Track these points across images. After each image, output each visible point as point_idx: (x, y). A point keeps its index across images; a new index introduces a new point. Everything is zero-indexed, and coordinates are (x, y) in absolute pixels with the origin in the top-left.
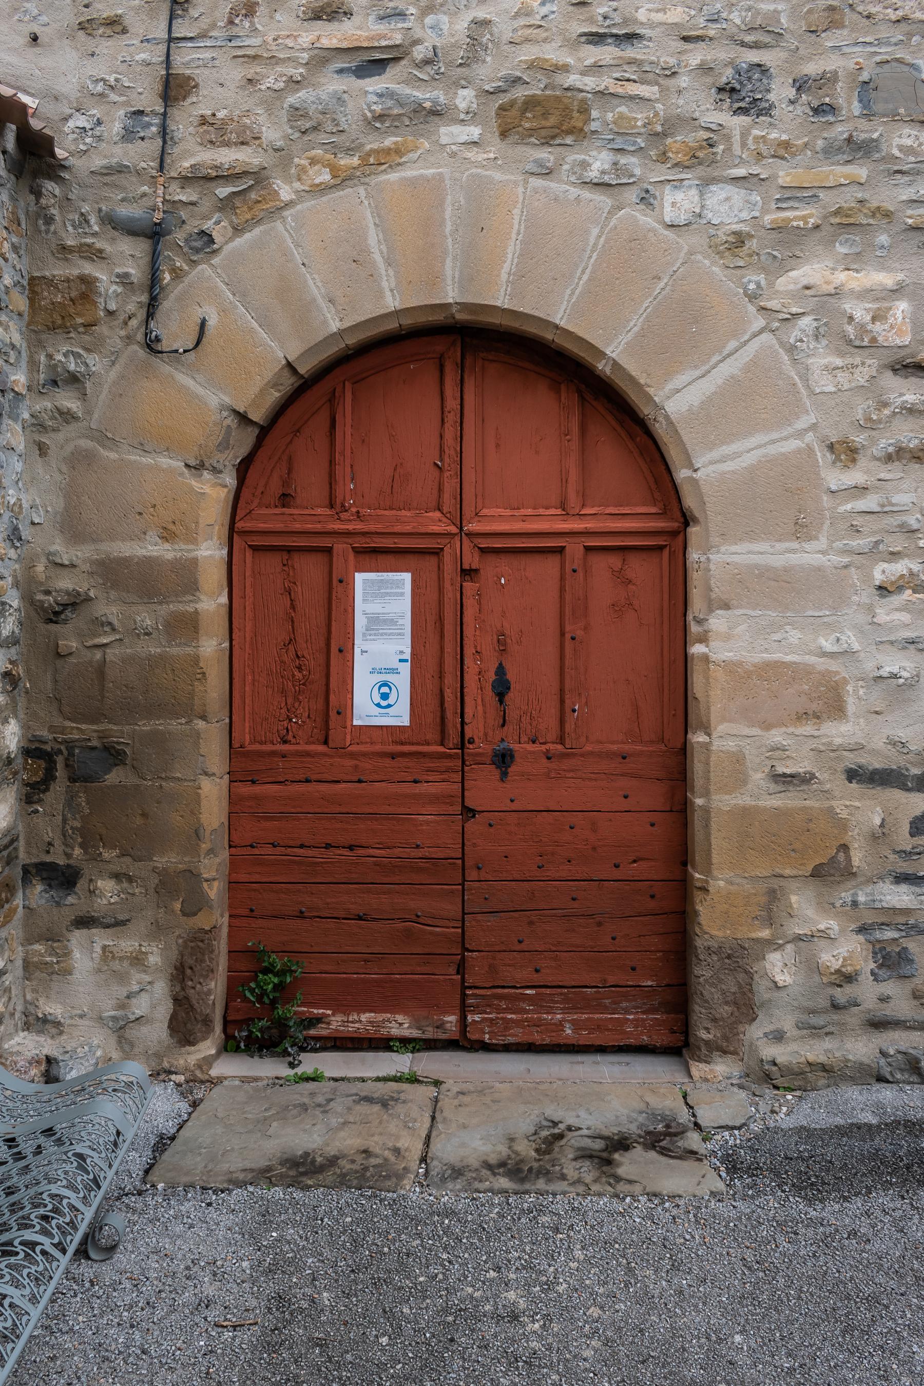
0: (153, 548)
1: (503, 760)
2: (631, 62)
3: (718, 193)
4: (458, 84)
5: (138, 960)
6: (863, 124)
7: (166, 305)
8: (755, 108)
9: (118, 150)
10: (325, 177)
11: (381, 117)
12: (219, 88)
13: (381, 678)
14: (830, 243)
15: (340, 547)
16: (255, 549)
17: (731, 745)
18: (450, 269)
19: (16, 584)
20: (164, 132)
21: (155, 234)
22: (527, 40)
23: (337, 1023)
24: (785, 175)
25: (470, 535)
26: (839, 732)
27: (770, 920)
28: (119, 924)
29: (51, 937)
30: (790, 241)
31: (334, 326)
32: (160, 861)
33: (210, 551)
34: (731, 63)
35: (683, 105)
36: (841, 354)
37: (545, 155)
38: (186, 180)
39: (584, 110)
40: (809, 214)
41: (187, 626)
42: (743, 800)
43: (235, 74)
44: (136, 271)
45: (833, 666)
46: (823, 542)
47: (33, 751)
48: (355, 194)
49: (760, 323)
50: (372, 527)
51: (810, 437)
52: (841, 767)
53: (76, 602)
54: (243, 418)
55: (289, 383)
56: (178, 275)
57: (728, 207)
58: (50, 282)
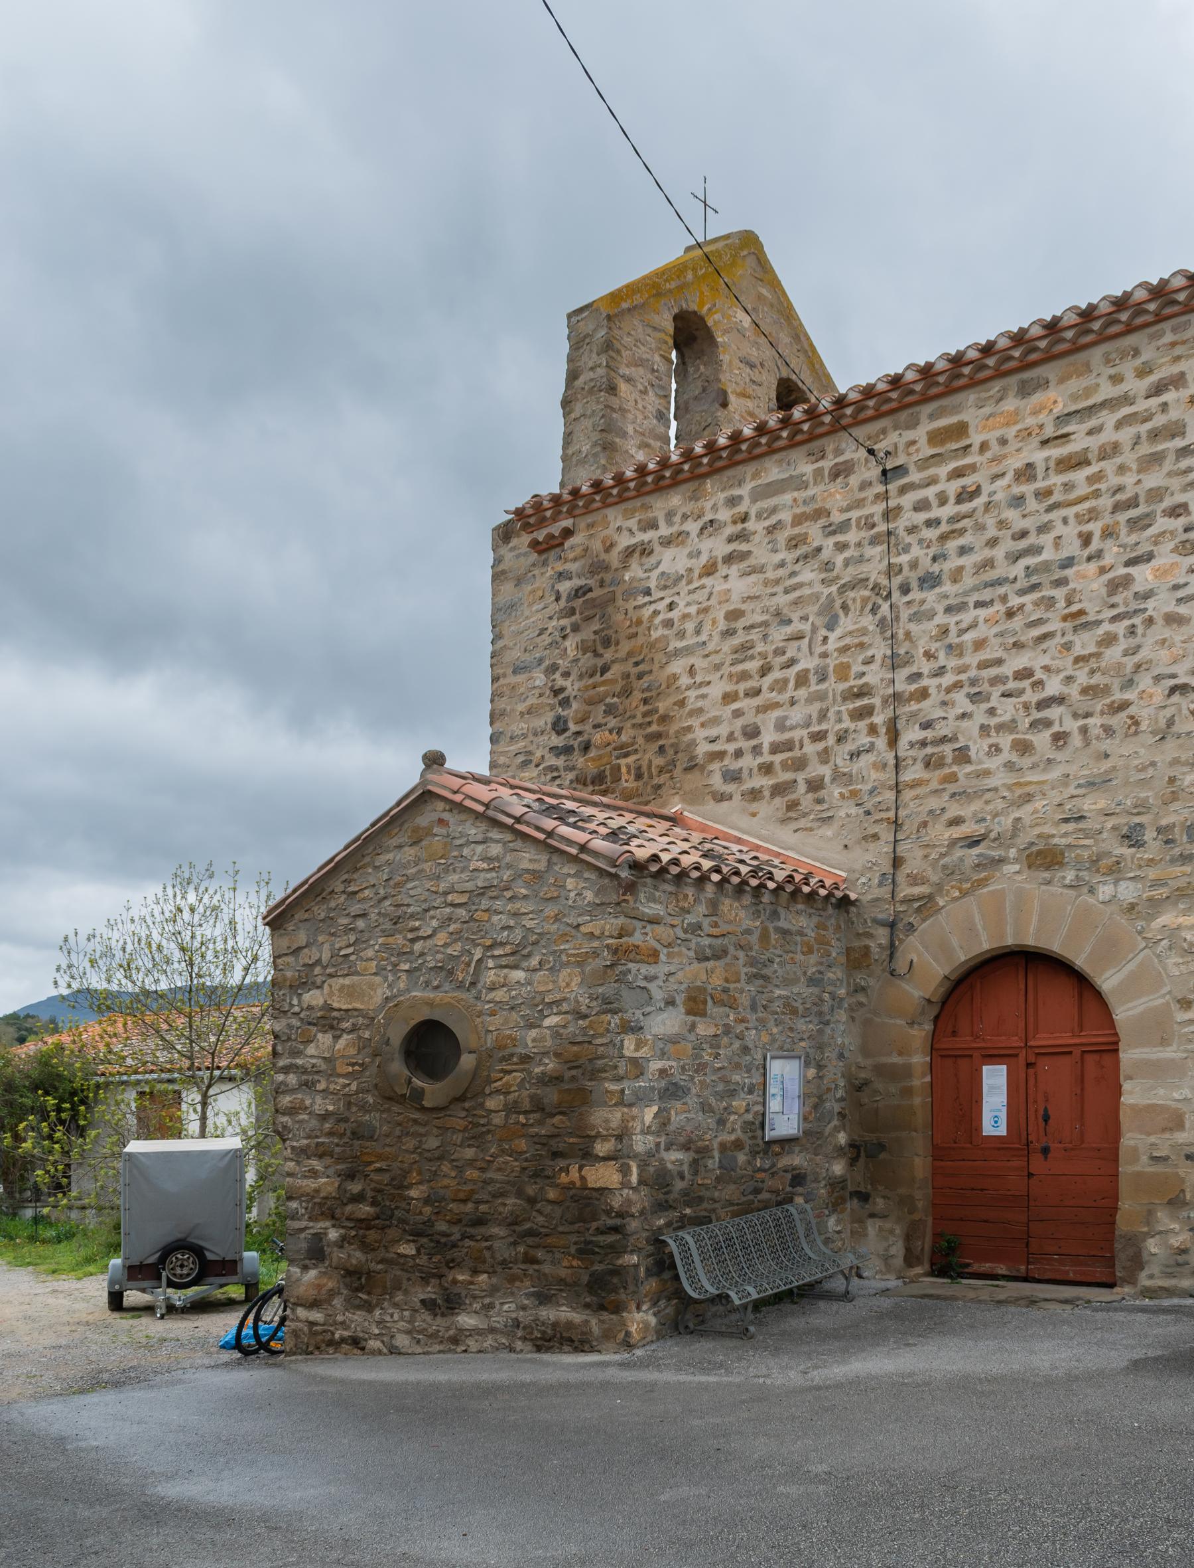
0: (895, 1059)
1: (1045, 1151)
2: (1080, 830)
3: (1123, 884)
4: (1009, 847)
5: (892, 1232)
6: (1188, 846)
7: (898, 954)
8: (1138, 844)
9: (876, 891)
10: (957, 894)
11: (978, 866)
12: (914, 863)
13: (994, 1117)
14: (1176, 904)
15: (976, 1054)
16: (942, 1056)
17: (1132, 1143)
18: (1009, 930)
19: (843, 1076)
20: (894, 882)
21: (892, 925)
22: (1037, 825)
23: (976, 1267)
24: (1152, 874)
25: (1031, 1047)
26: (1181, 1137)
27: (1148, 1224)
28: (886, 1217)
29: (861, 1221)
30: (1155, 906)
31: (963, 959)
32: (901, 1191)
33: (919, 1059)
34: (1127, 824)
35: (1103, 846)
36: (1182, 957)
37: (1047, 875)
38: (902, 902)
39: (1062, 854)
40: (1163, 892)
41: (908, 1092)
42: (1138, 1168)
43: (920, 853)
44: (884, 941)
45: (1180, 1105)
46: (1174, 1047)
47: (852, 1145)
48: (970, 899)
49: (1144, 944)
50: (989, 1045)
51: (1168, 997)
52: (1183, 1153)
53: (866, 1083)
54: (929, 1001)
55: (948, 984)
56: (901, 941)
57: (1128, 891)
58: (853, 949)
